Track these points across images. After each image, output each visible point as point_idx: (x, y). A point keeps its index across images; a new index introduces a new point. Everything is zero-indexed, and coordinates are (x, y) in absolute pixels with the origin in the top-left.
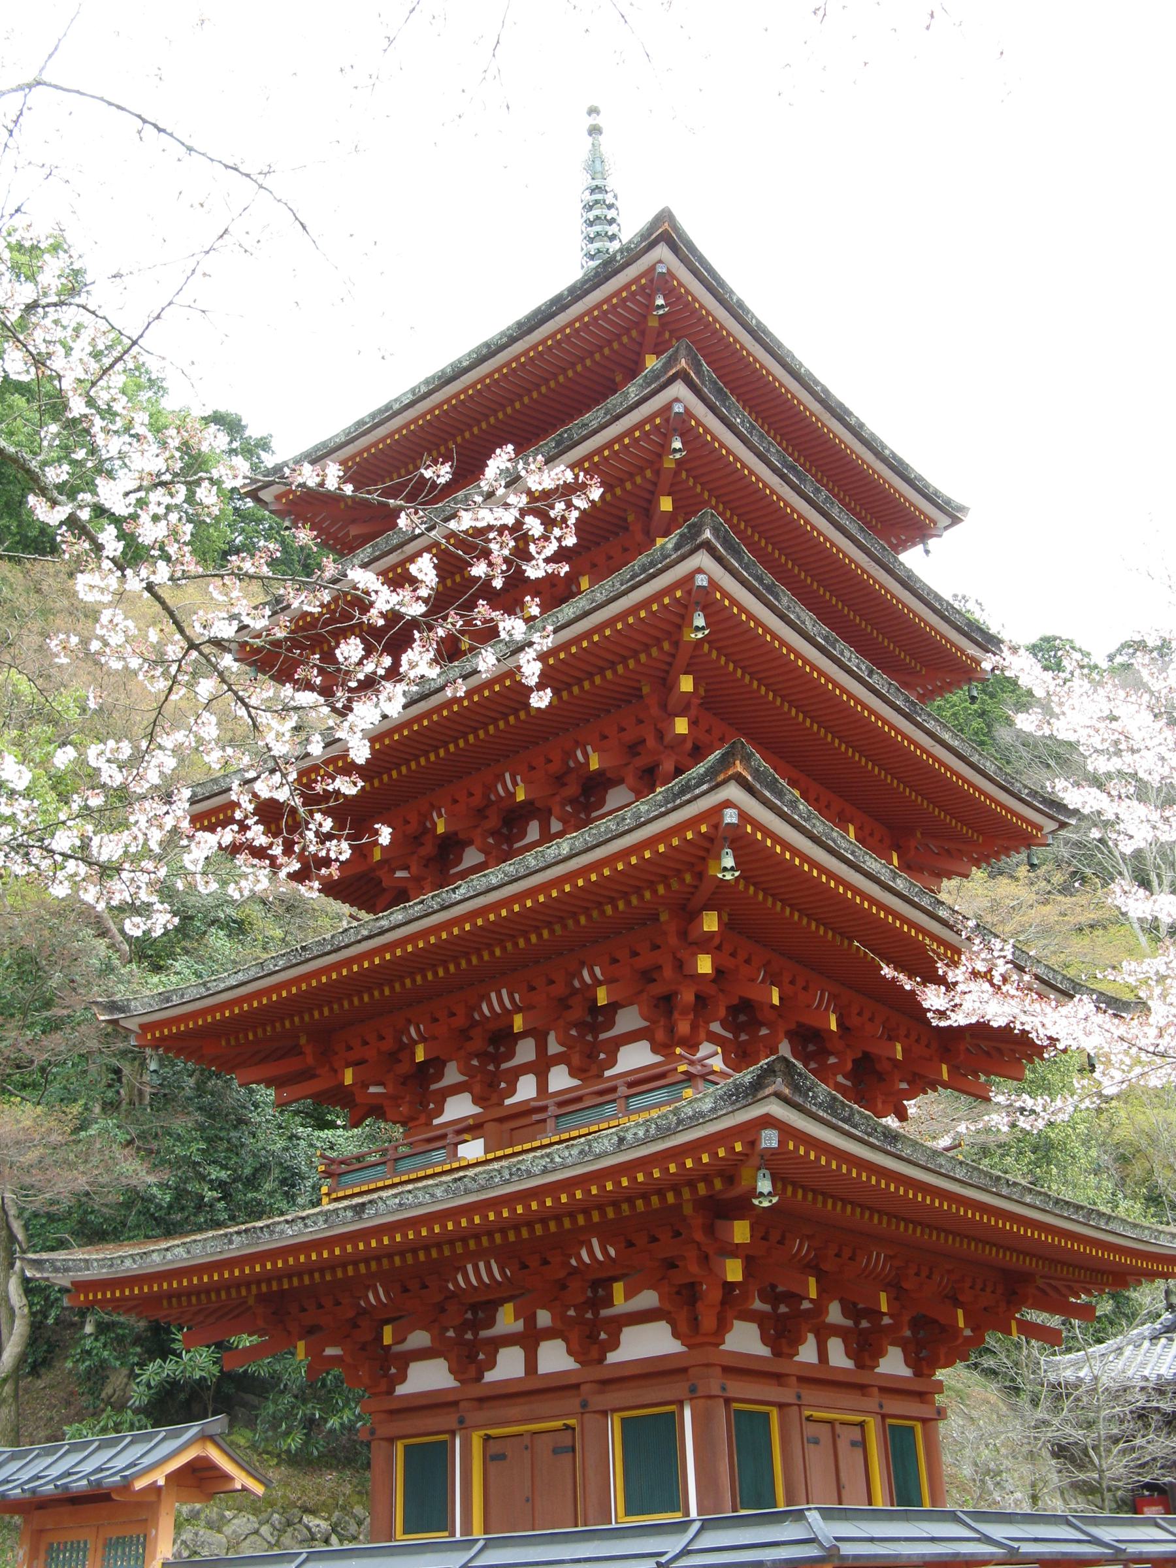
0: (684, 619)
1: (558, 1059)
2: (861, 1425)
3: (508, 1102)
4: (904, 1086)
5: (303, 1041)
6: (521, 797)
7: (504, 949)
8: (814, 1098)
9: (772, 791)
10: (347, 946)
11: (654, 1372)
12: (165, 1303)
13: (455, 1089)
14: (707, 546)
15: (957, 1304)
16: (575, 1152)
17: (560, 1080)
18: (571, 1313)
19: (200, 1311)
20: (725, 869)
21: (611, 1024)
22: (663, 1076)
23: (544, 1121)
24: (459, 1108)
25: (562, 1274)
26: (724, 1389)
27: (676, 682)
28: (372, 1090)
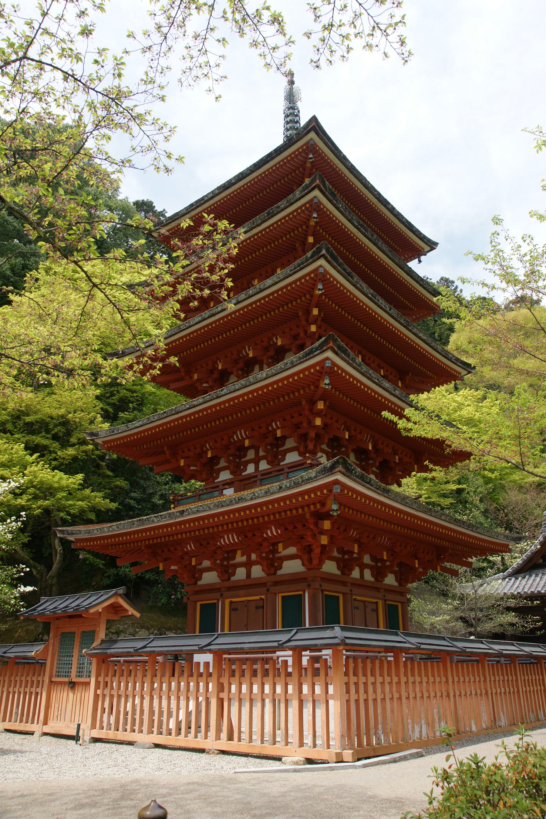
0: (314, 286)
1: (263, 458)
3: (243, 474)
4: (400, 473)
5: (165, 449)
6: (251, 355)
7: (241, 414)
8: (355, 473)
9: (345, 354)
10: (181, 412)
11: (294, 579)
12: (110, 547)
13: (224, 469)
14: (323, 256)
15: (416, 558)
16: (263, 492)
17: (264, 465)
18: (264, 555)
19: (124, 551)
21: (284, 444)
22: (302, 464)
23: (256, 481)
24: (225, 476)
25: (260, 540)
26: (321, 586)
27: (312, 311)
28: (192, 468)
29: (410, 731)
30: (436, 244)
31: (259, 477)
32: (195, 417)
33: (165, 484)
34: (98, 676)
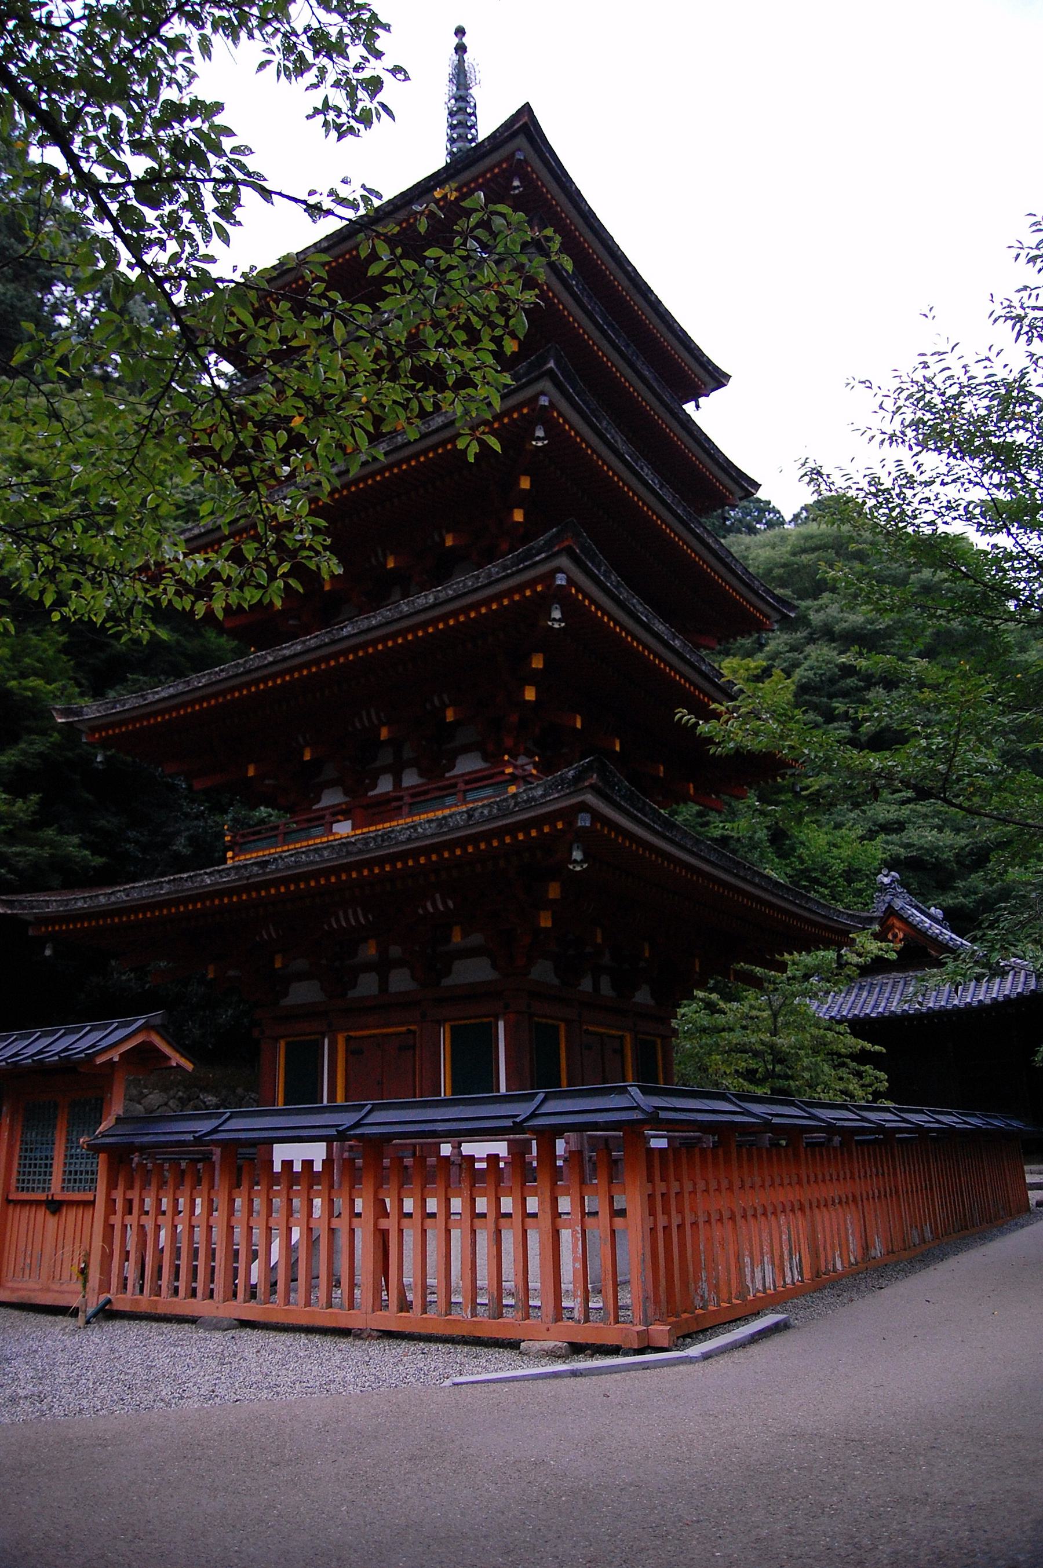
2: (621, 1038)
3: (371, 794)
8: (619, 791)
20: (554, 620)
23: (400, 808)
29: (748, 1278)
30: (728, 377)
31: (407, 799)
32: (415, 636)
33: (197, 818)
34: (112, 1185)
